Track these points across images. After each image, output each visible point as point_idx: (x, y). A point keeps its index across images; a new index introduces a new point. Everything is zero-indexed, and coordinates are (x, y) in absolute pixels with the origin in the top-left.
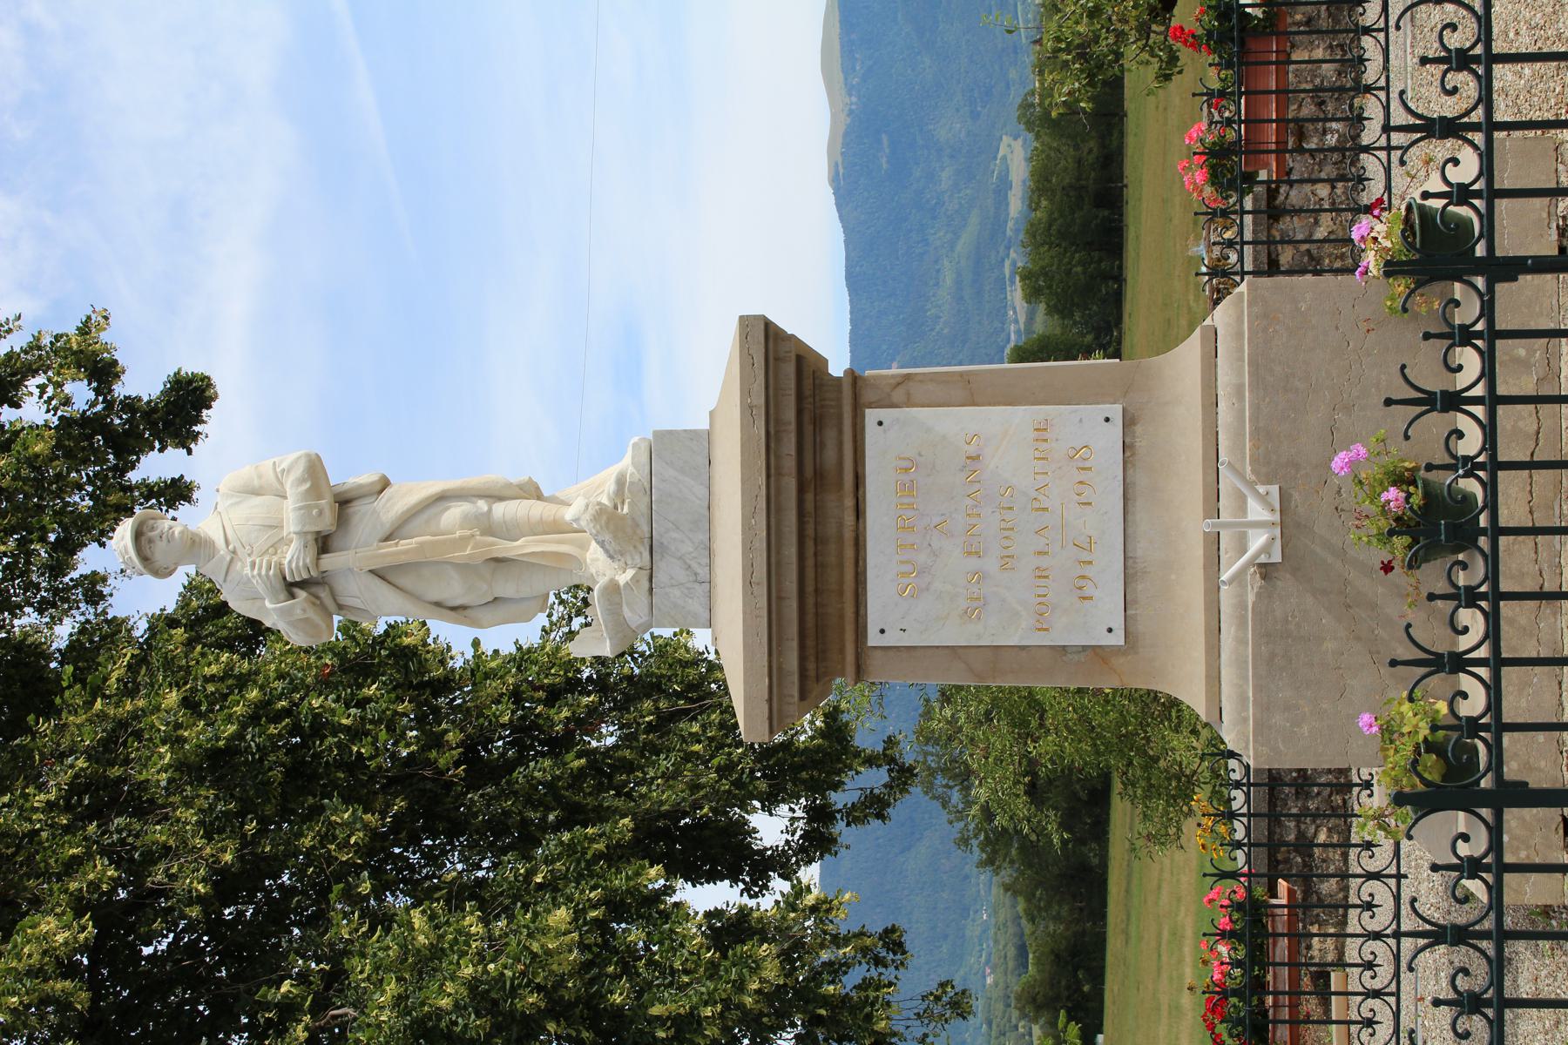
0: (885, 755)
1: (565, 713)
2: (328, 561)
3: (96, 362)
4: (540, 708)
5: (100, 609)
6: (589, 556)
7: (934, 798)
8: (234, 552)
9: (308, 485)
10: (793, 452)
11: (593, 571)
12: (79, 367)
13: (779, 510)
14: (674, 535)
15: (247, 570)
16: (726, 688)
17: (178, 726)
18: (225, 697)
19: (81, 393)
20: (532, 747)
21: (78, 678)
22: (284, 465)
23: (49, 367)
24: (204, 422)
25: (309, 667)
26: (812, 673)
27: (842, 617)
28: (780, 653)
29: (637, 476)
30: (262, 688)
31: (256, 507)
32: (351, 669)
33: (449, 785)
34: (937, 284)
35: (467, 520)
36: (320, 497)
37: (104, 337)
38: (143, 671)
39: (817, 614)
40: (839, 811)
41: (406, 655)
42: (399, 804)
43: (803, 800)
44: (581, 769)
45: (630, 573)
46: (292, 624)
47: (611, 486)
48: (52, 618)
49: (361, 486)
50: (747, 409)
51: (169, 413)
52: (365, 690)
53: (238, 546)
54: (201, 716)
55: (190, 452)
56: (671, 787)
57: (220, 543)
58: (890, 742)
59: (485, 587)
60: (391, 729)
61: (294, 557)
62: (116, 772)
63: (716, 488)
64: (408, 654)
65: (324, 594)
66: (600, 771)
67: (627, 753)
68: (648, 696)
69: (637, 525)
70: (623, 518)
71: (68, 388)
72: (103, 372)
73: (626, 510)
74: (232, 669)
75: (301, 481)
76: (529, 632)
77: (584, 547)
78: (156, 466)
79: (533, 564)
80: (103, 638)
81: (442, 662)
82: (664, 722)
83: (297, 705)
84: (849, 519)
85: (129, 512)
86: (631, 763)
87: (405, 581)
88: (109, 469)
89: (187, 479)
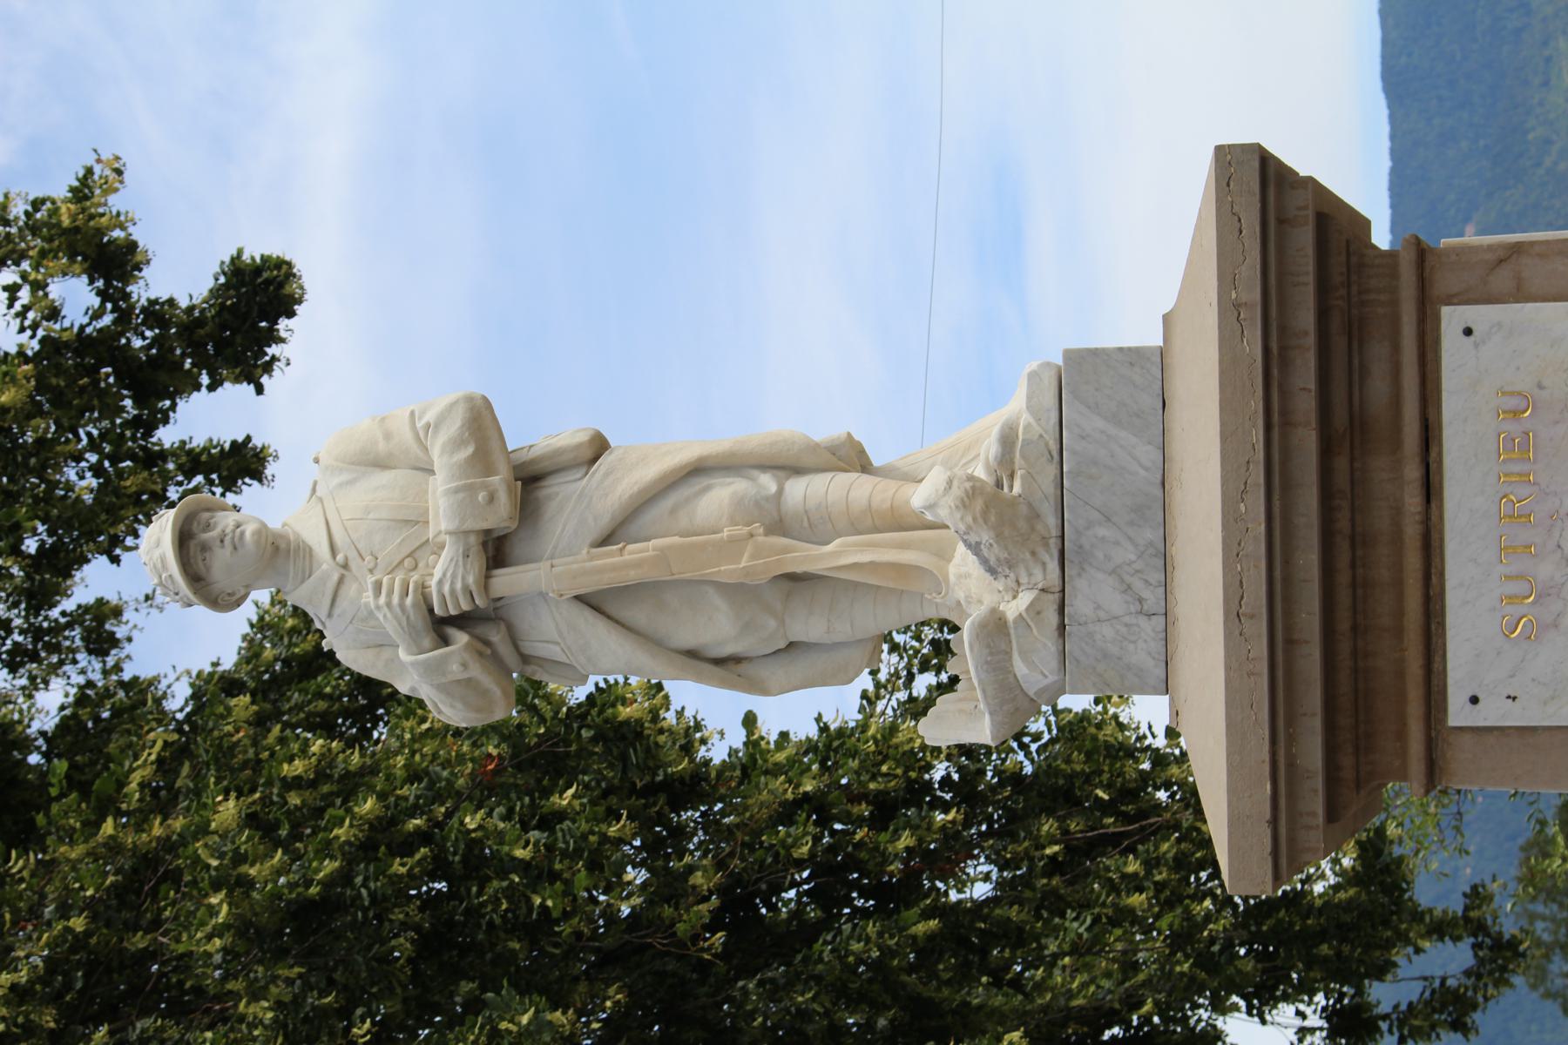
0: (1466, 919)
1: (906, 840)
2: (507, 581)
3: (102, 246)
4: (859, 835)
5: (110, 661)
6: (952, 570)
7: (1548, 995)
8: (345, 566)
9: (470, 450)
10: (1312, 386)
11: (960, 595)
12: (72, 259)
13: (1287, 487)
14: (1102, 531)
15: (368, 597)
16: (1195, 793)
17: (239, 858)
18: (319, 812)
19: (76, 297)
20: (849, 902)
21: (77, 782)
22: (430, 416)
23: (23, 256)
24: (283, 341)
25: (461, 759)
26: (1348, 774)
27: (1400, 674)
28: (1291, 739)
29: (1037, 429)
30: (382, 796)
31: (379, 489)
32: (532, 763)
33: (703, 967)
34: (1546, 83)
35: (746, 511)
36: (489, 470)
37: (116, 202)
38: (186, 769)
39: (1355, 670)
40: (1385, 1017)
41: (623, 738)
42: (614, 997)
43: (1320, 998)
44: (931, 937)
45: (1025, 599)
46: (442, 688)
47: (990, 448)
48: (32, 679)
49: (559, 452)
50: (1230, 310)
51: (224, 327)
52: (555, 799)
53: (352, 554)
54: (278, 843)
55: (260, 390)
56: (1088, 967)
57: (322, 550)
58: (1477, 895)
59: (772, 623)
60: (594, 866)
61: (447, 574)
62: (139, 941)
63: (1177, 448)
64: (631, 733)
65: (497, 636)
66: (963, 942)
67: (1013, 912)
68: (1050, 812)
69: (1039, 511)
70: (1013, 502)
71: (56, 290)
72: (113, 262)
73: (1017, 489)
74: (331, 765)
75: (457, 444)
76: (841, 704)
77: (945, 555)
78: (204, 416)
79: (856, 585)
80: (117, 712)
81: (688, 749)
82: (1081, 852)
83: (440, 825)
84: (1412, 502)
85: (160, 499)
86: (1020, 929)
87: (638, 615)
88: (126, 424)
89: (257, 442)
